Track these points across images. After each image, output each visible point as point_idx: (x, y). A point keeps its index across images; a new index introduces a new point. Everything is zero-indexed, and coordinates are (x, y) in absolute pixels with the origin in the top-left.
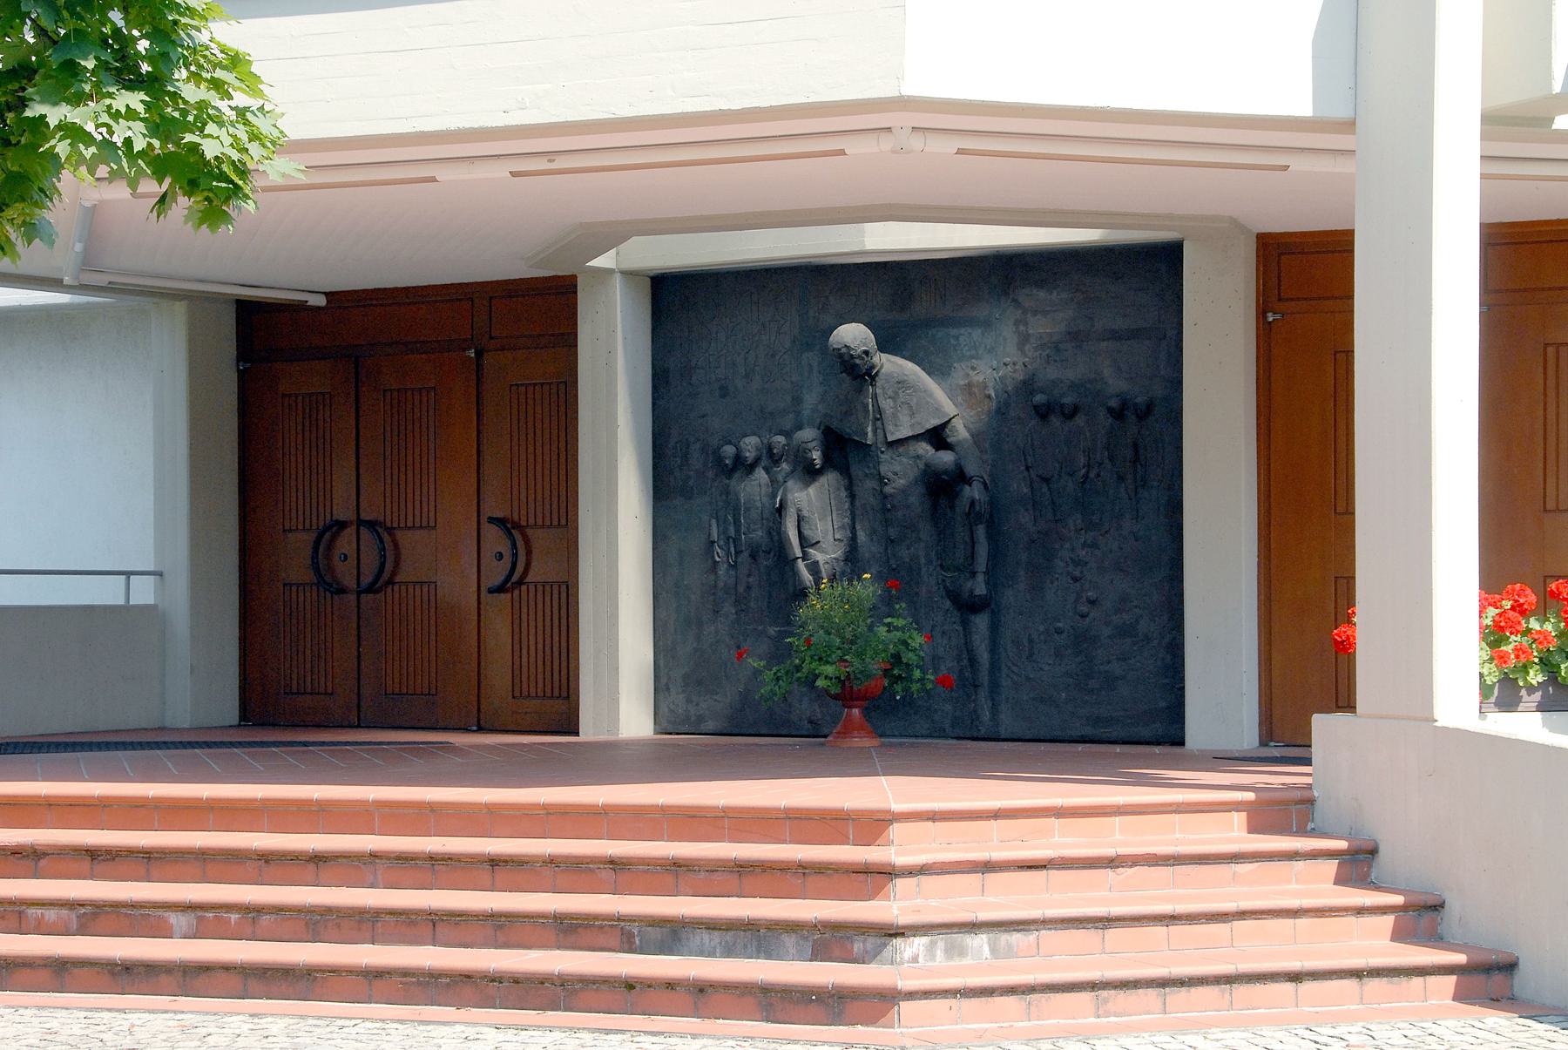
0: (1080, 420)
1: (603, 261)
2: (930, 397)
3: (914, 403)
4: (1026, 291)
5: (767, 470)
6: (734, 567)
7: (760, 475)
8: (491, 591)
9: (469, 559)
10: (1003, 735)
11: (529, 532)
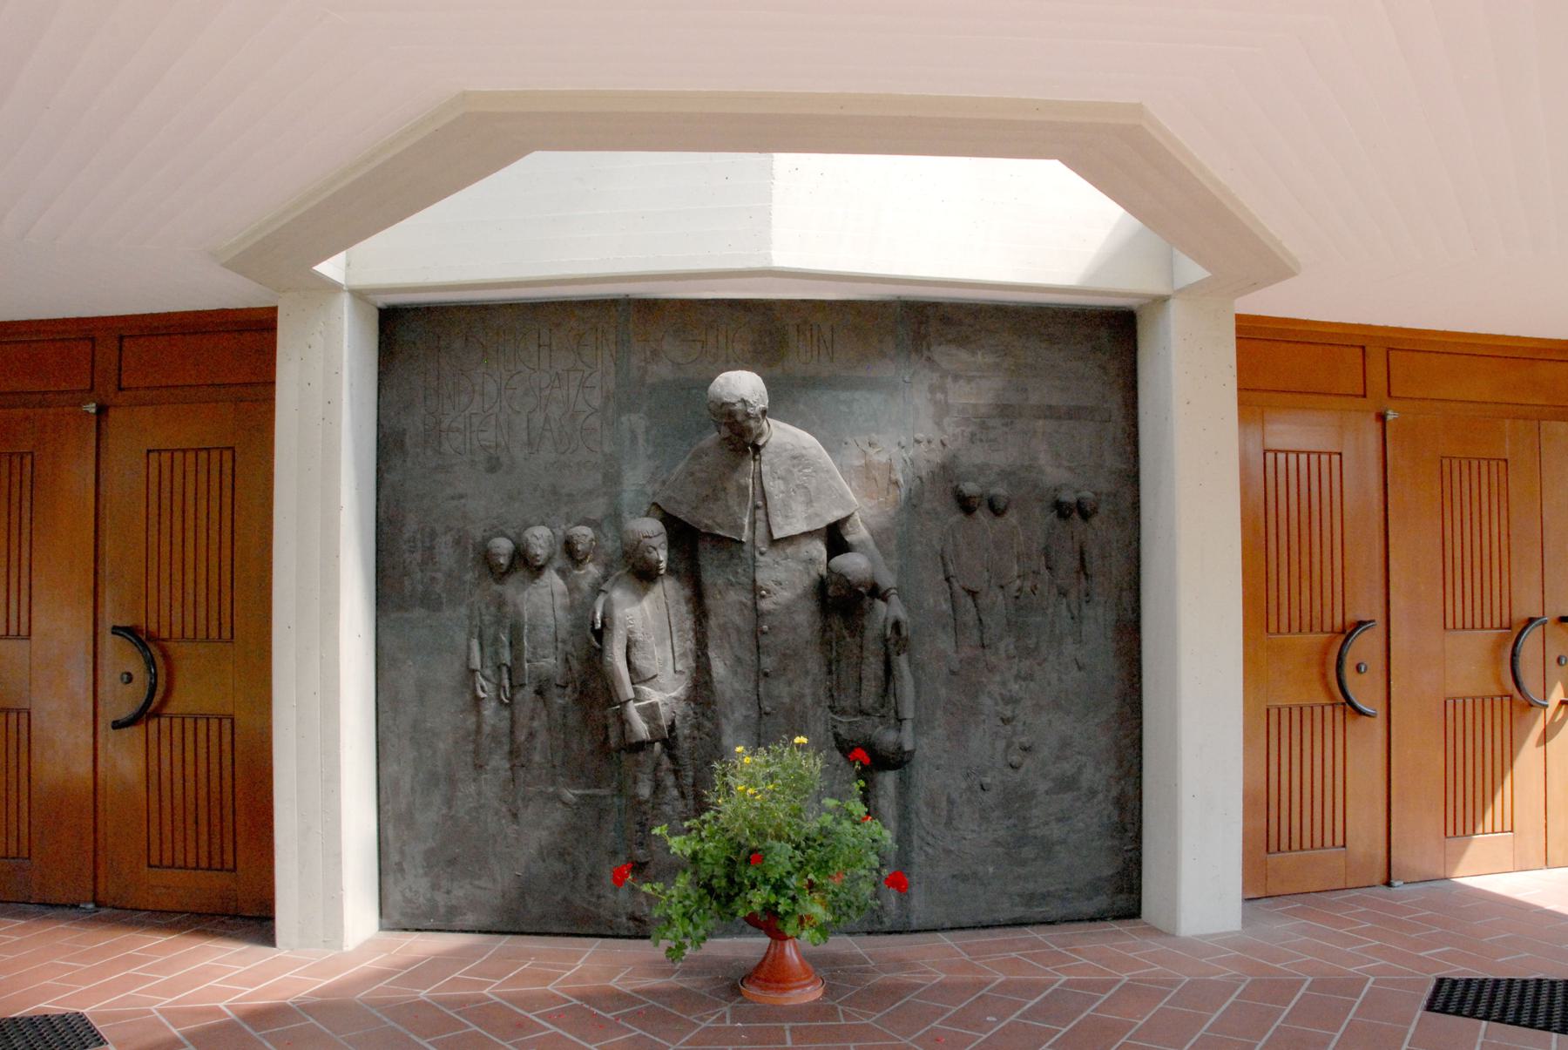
0: (1012, 518)
1: (331, 268)
2: (828, 474)
3: (812, 487)
4: (943, 348)
5: (562, 573)
6: (510, 705)
7: (552, 580)
8: (117, 725)
9: (80, 680)
10: (915, 924)
11: (171, 646)
